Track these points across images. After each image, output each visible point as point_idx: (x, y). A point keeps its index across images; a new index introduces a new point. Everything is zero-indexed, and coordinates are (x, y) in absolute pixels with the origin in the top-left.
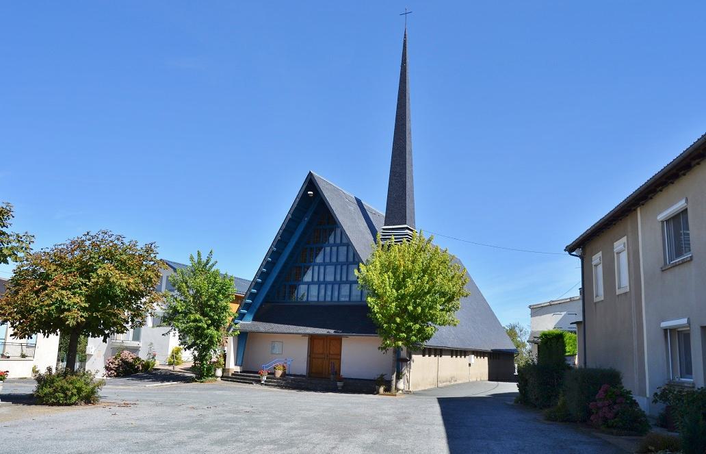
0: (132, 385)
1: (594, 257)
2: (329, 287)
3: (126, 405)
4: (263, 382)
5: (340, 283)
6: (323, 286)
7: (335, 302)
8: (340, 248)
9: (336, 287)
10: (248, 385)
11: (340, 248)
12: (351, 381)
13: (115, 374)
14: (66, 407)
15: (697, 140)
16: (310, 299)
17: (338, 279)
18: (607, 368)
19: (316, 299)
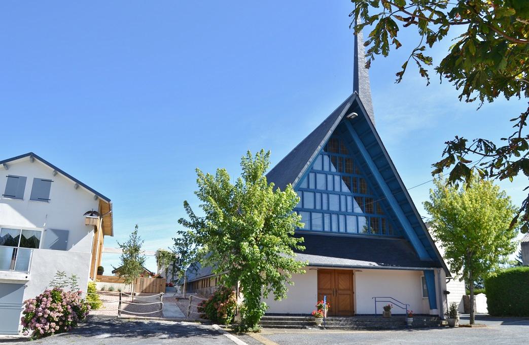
0: (3, 224)
1: (146, 323)
2: (334, 217)
3: (479, 108)
4: (320, 325)
5: (346, 214)
6: (327, 217)
7: (342, 233)
8: (323, 188)
9: (342, 218)
10: (277, 329)
11: (323, 188)
12: (393, 327)
13: (58, 328)
14: (364, 313)
15: (518, 173)
16: (314, 228)
17: (343, 209)
18: (149, 339)
19: (320, 229)
